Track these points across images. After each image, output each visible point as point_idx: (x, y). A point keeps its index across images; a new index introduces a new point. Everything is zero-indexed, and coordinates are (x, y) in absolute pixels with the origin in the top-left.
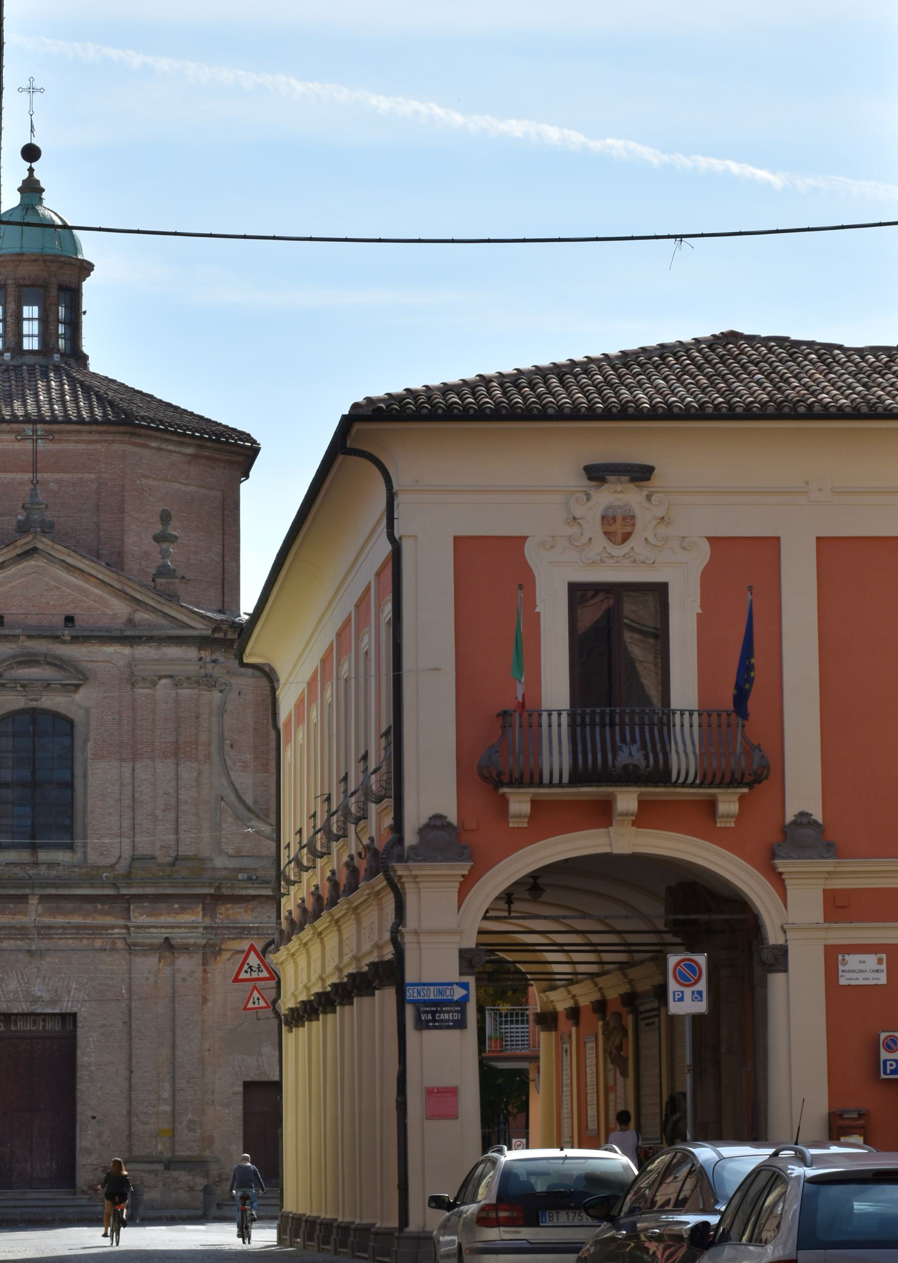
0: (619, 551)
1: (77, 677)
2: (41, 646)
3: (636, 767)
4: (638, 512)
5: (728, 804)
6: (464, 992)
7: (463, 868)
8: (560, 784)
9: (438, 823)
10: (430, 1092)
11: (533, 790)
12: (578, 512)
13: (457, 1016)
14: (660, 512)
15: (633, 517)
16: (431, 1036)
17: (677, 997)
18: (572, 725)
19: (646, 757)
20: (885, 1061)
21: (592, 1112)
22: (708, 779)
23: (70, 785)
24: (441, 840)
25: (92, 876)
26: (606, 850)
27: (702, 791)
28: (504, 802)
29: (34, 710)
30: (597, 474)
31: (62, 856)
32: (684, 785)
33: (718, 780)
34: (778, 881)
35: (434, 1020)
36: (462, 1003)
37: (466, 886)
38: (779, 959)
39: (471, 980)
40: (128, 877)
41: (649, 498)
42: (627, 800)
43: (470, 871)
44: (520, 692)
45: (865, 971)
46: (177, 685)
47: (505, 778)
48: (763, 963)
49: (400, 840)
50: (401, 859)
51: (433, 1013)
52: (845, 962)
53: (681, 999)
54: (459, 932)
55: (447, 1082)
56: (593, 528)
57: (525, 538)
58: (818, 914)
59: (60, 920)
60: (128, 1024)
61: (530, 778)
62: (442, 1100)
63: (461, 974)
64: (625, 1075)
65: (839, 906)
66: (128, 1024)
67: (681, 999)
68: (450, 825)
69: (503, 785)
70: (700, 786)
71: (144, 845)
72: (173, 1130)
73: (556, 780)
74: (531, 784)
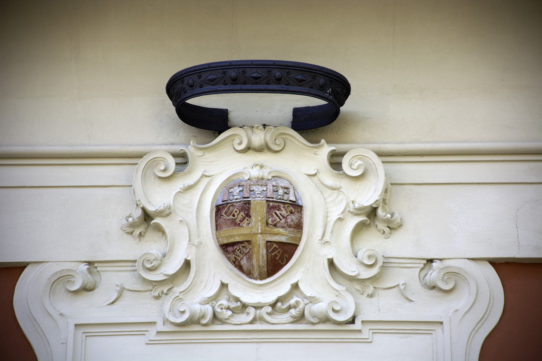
0: (260, 293)
4: (308, 195)
12: (158, 198)
14: (368, 195)
15: (296, 207)
30: (197, 103)
41: (335, 161)
56: (192, 234)
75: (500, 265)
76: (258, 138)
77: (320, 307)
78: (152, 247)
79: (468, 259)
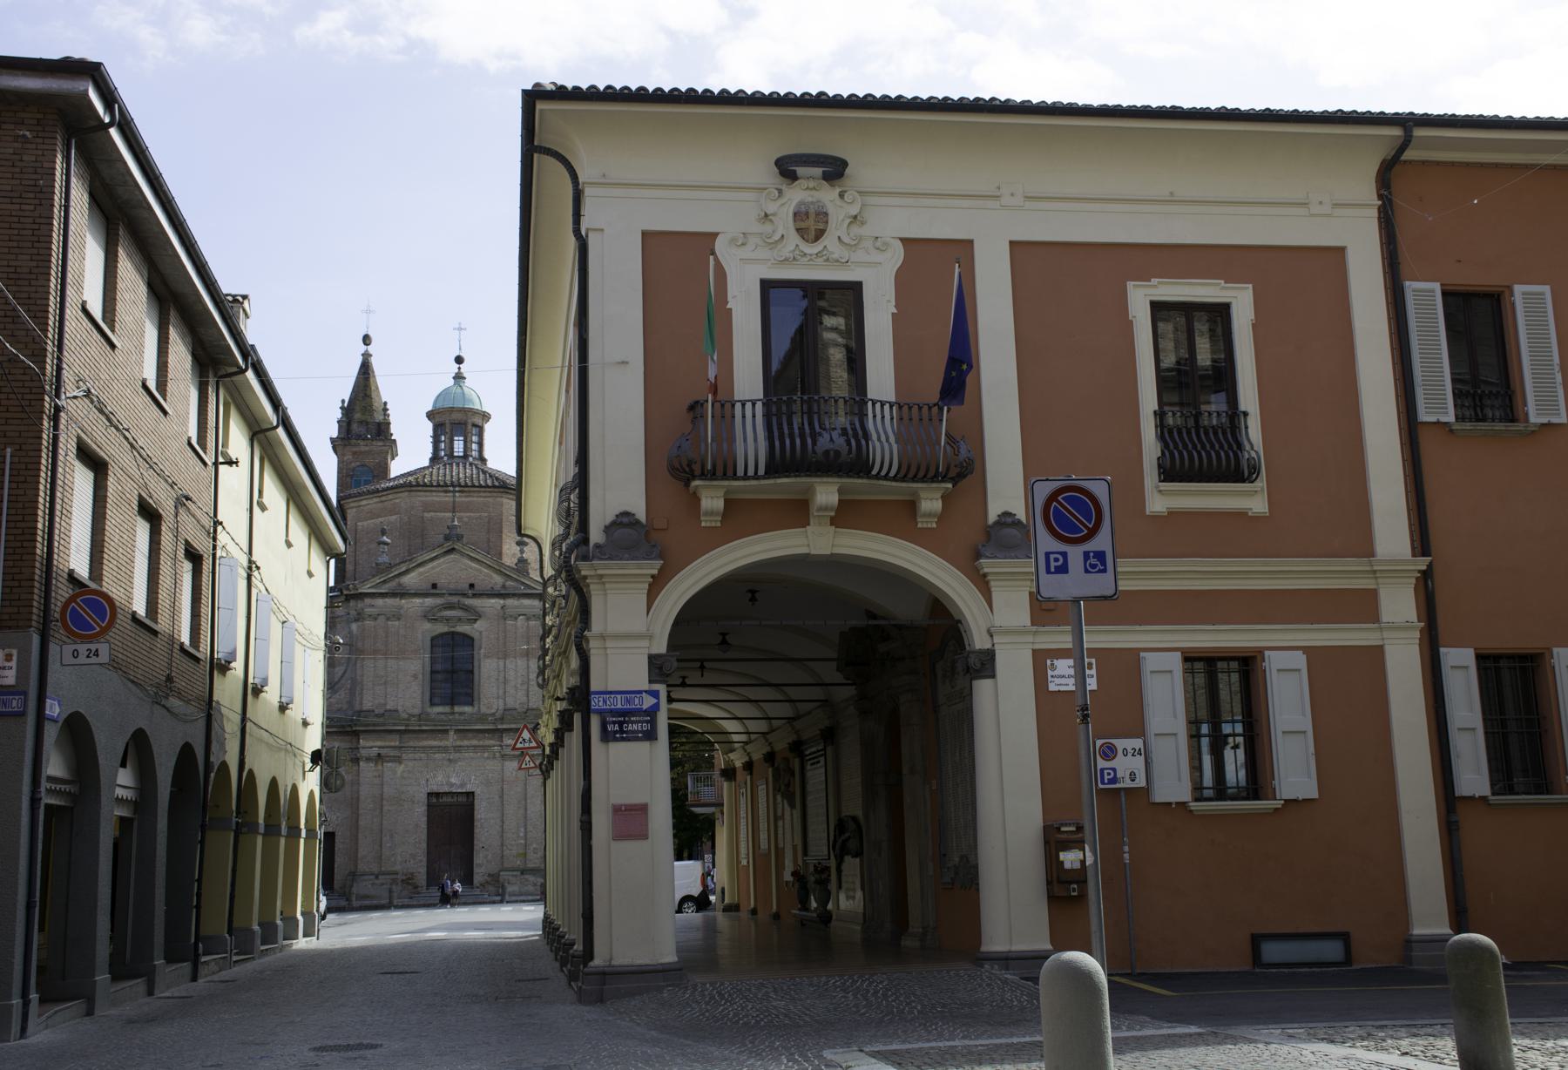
0: (812, 249)
1: (475, 616)
2: (455, 599)
3: (837, 453)
4: (831, 209)
5: (931, 502)
6: (654, 701)
7: (653, 568)
8: (756, 477)
9: (625, 520)
10: (617, 810)
11: (726, 483)
12: (771, 208)
13: (646, 727)
14: (854, 210)
15: (826, 214)
16: (617, 748)
17: (1053, 564)
18: (767, 416)
19: (849, 443)
20: (1102, 770)
21: (763, 836)
22: (908, 473)
23: (472, 672)
24: (630, 536)
25: (482, 718)
26: (804, 550)
27: (904, 485)
28: (695, 499)
29: (453, 633)
30: (787, 169)
31: (467, 709)
32: (886, 478)
33: (921, 474)
34: (983, 584)
35: (622, 731)
36: (652, 712)
37: (656, 586)
38: (986, 665)
39: (662, 689)
40: (502, 719)
41: (841, 195)
42: (826, 493)
43: (660, 571)
44: (711, 375)
45: (1062, 676)
46: (528, 619)
47: (697, 469)
48: (968, 670)
49: (586, 541)
50: (585, 558)
51: (621, 724)
52: (1053, 667)
53: (1063, 569)
54: (651, 637)
55: (636, 799)
56: (784, 223)
57: (715, 235)
58: (1024, 618)
59: (466, 743)
60: (501, 797)
61: (724, 470)
62: (631, 820)
63: (650, 682)
64: (792, 806)
65: (1043, 610)
66: (501, 797)
67: (1063, 569)
68: (638, 522)
69: (694, 478)
70: (903, 479)
71: (511, 703)
72: (525, 854)
73: (751, 472)
74: (725, 477)
75: (903, 240)
76: (812, 184)
77: (835, 256)
78: (768, 228)
79: (366, 370)
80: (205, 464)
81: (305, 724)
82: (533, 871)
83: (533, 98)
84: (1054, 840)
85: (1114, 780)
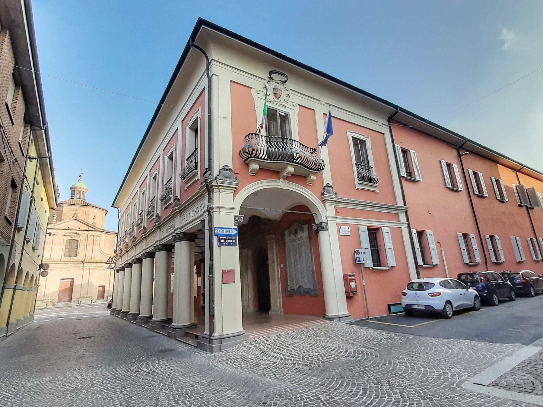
10: (224, 272)
56: (270, 91)
80: (23, 155)
81: (39, 256)
82: (89, 297)
83: (201, 22)
84: (347, 280)
85: (359, 261)
